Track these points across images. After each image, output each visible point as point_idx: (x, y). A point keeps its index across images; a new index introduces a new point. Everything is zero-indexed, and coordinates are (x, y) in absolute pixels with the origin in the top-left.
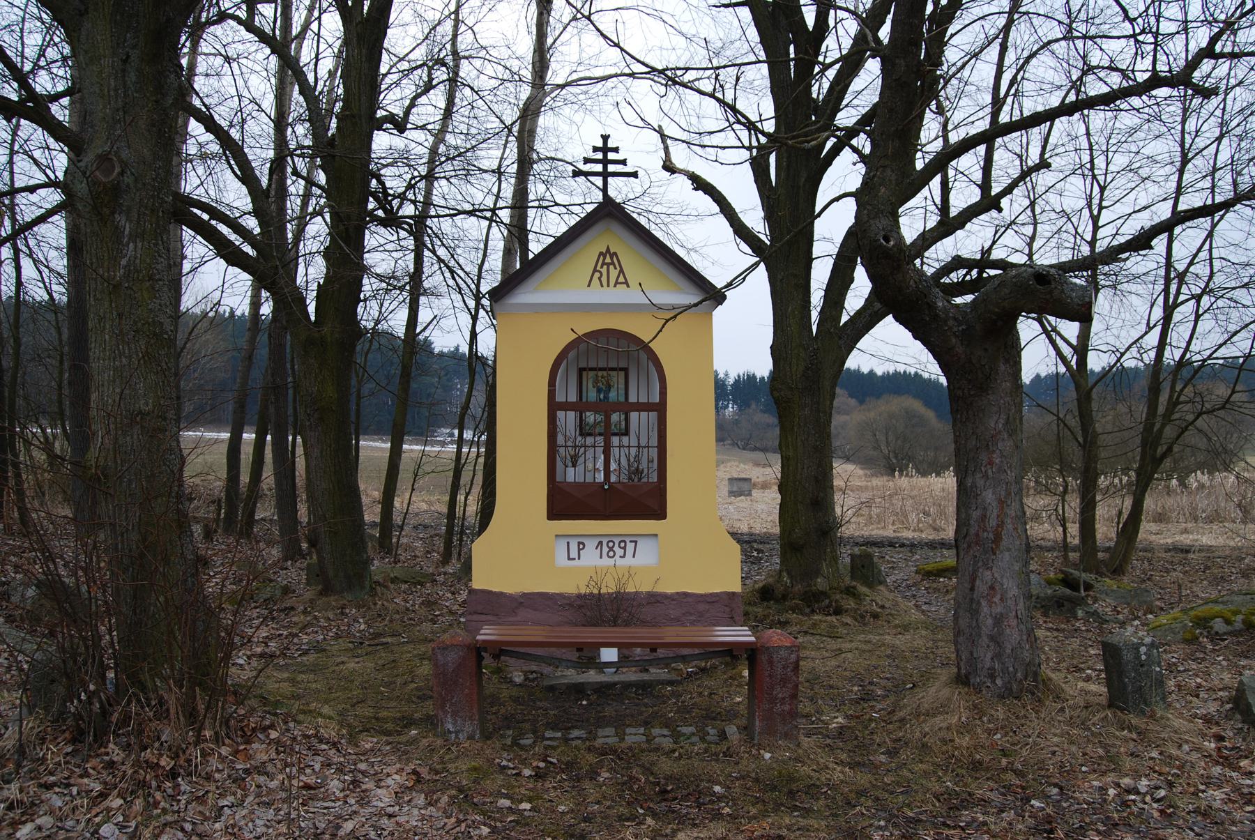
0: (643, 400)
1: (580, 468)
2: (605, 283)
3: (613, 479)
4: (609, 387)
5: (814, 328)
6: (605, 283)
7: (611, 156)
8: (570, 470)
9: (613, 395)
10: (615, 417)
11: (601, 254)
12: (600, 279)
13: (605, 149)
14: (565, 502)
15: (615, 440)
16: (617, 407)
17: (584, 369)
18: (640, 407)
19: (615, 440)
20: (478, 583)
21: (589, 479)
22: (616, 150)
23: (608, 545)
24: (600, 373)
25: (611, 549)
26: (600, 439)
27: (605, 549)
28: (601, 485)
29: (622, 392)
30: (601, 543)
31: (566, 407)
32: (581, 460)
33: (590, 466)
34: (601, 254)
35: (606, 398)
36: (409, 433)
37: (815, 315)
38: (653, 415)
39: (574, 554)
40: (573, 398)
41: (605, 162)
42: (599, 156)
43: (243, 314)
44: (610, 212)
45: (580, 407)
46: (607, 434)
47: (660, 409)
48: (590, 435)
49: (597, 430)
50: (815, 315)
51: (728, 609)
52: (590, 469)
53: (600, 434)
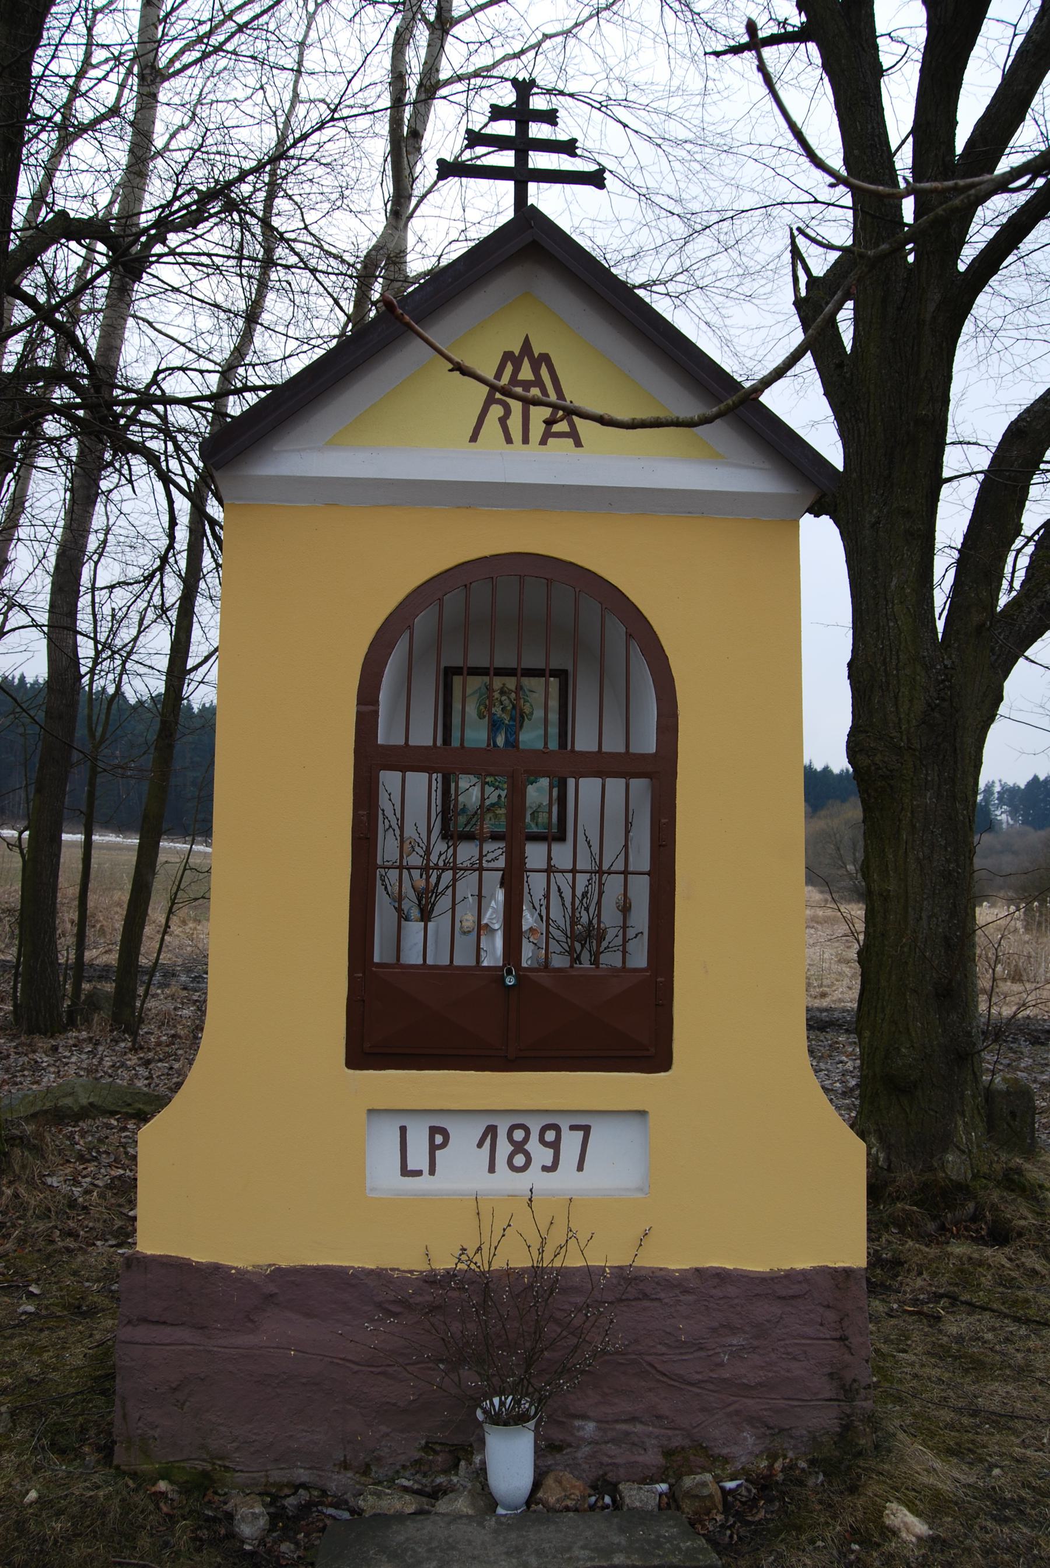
0: (613, 744)
1: (440, 924)
2: (516, 432)
3: (528, 954)
4: (519, 718)
5: (940, 625)
6: (516, 432)
7: (538, 131)
8: (414, 929)
9: (530, 737)
10: (538, 793)
11: (508, 356)
12: (503, 421)
13: (521, 113)
14: (398, 1020)
15: (535, 854)
16: (537, 765)
17: (457, 671)
18: (602, 765)
19: (535, 854)
20: (150, 1241)
21: (463, 959)
22: (550, 117)
23: (511, 1138)
24: (498, 682)
25: (519, 1147)
26: (496, 853)
27: (504, 1148)
28: (495, 975)
29: (554, 731)
30: (491, 1131)
31: (405, 759)
32: (444, 903)
33: (468, 919)
34: (508, 356)
35: (512, 743)
36: (165, 833)
37: (941, 597)
38: (640, 786)
39: (418, 1159)
40: (423, 736)
41: (522, 145)
42: (506, 128)
43: (36, 682)
44: (530, 245)
45: (443, 761)
46: (515, 837)
47: (659, 771)
48: (469, 837)
49: (489, 826)
50: (941, 597)
51: (831, 1316)
52: (465, 931)
53: (495, 837)
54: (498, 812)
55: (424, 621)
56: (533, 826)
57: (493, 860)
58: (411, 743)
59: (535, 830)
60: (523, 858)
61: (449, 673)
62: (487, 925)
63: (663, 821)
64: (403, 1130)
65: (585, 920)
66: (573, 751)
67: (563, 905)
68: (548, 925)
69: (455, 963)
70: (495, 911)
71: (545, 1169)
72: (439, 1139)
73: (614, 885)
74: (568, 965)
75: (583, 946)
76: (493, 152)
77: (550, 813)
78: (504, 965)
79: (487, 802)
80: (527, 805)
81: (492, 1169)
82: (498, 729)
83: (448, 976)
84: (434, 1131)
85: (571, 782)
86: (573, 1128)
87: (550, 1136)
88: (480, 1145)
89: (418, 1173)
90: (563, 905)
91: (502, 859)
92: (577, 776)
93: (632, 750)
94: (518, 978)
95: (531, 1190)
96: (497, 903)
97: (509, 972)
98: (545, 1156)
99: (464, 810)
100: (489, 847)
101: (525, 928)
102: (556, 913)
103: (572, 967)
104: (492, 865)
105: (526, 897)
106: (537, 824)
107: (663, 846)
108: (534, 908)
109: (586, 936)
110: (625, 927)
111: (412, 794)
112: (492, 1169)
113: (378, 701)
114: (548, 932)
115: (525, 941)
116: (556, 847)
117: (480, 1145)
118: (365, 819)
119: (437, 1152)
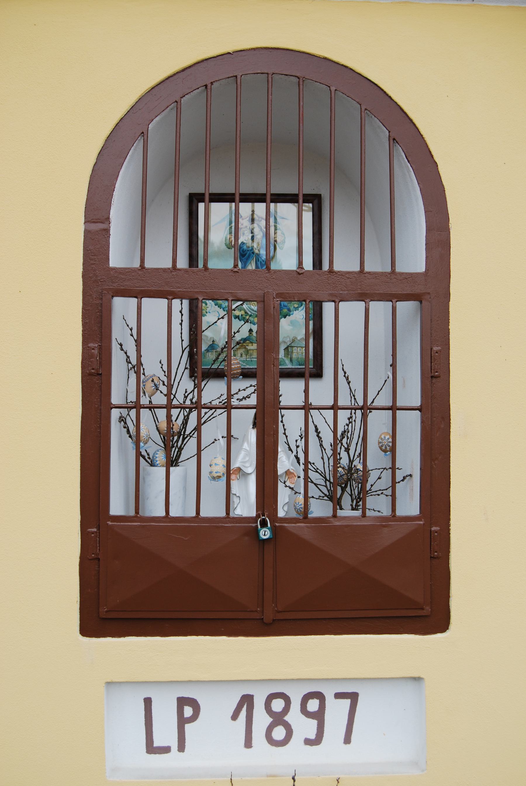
0: (376, 264)
3: (286, 503)
10: (293, 326)
15: (290, 391)
18: (364, 288)
19: (290, 391)
21: (212, 508)
25: (278, 719)
26: (245, 389)
28: (248, 528)
30: (247, 700)
31: (142, 284)
32: (190, 448)
38: (406, 309)
39: (165, 732)
46: (267, 374)
47: (428, 294)
49: (238, 361)
52: (208, 482)
53: (246, 374)
54: (250, 347)
55: (158, 128)
56: (287, 361)
57: (244, 398)
58: (147, 265)
59: (290, 366)
60: (277, 396)
61: (195, 199)
62: (239, 469)
63: (435, 349)
64: (148, 702)
65: (344, 461)
66: (331, 271)
67: (321, 445)
68: (306, 470)
69: (203, 514)
70: (248, 453)
71: (308, 742)
72: (188, 711)
73: (379, 423)
74: (330, 513)
75: (343, 490)
78: (258, 516)
79: (238, 337)
80: (281, 339)
81: (248, 743)
82: (247, 259)
83: (196, 528)
84: (182, 702)
85: (328, 308)
86: (339, 696)
87: (313, 705)
88: (235, 717)
89: (166, 750)
90: (321, 445)
91: (254, 397)
92: (337, 299)
93: (399, 269)
94: (274, 530)
95: (293, 779)
96: (250, 445)
97: (264, 524)
98: (310, 727)
99: (212, 346)
100: (237, 385)
101: (281, 470)
102: (314, 456)
103: (335, 516)
104: (244, 403)
105: (281, 438)
106: (291, 360)
107: (436, 377)
108: (290, 449)
109: (348, 482)
110: (393, 468)
111: (152, 329)
112: (248, 743)
113: (108, 218)
114: (307, 478)
115: (280, 486)
116: (313, 384)
117: (235, 717)
118: (96, 352)
119: (187, 727)
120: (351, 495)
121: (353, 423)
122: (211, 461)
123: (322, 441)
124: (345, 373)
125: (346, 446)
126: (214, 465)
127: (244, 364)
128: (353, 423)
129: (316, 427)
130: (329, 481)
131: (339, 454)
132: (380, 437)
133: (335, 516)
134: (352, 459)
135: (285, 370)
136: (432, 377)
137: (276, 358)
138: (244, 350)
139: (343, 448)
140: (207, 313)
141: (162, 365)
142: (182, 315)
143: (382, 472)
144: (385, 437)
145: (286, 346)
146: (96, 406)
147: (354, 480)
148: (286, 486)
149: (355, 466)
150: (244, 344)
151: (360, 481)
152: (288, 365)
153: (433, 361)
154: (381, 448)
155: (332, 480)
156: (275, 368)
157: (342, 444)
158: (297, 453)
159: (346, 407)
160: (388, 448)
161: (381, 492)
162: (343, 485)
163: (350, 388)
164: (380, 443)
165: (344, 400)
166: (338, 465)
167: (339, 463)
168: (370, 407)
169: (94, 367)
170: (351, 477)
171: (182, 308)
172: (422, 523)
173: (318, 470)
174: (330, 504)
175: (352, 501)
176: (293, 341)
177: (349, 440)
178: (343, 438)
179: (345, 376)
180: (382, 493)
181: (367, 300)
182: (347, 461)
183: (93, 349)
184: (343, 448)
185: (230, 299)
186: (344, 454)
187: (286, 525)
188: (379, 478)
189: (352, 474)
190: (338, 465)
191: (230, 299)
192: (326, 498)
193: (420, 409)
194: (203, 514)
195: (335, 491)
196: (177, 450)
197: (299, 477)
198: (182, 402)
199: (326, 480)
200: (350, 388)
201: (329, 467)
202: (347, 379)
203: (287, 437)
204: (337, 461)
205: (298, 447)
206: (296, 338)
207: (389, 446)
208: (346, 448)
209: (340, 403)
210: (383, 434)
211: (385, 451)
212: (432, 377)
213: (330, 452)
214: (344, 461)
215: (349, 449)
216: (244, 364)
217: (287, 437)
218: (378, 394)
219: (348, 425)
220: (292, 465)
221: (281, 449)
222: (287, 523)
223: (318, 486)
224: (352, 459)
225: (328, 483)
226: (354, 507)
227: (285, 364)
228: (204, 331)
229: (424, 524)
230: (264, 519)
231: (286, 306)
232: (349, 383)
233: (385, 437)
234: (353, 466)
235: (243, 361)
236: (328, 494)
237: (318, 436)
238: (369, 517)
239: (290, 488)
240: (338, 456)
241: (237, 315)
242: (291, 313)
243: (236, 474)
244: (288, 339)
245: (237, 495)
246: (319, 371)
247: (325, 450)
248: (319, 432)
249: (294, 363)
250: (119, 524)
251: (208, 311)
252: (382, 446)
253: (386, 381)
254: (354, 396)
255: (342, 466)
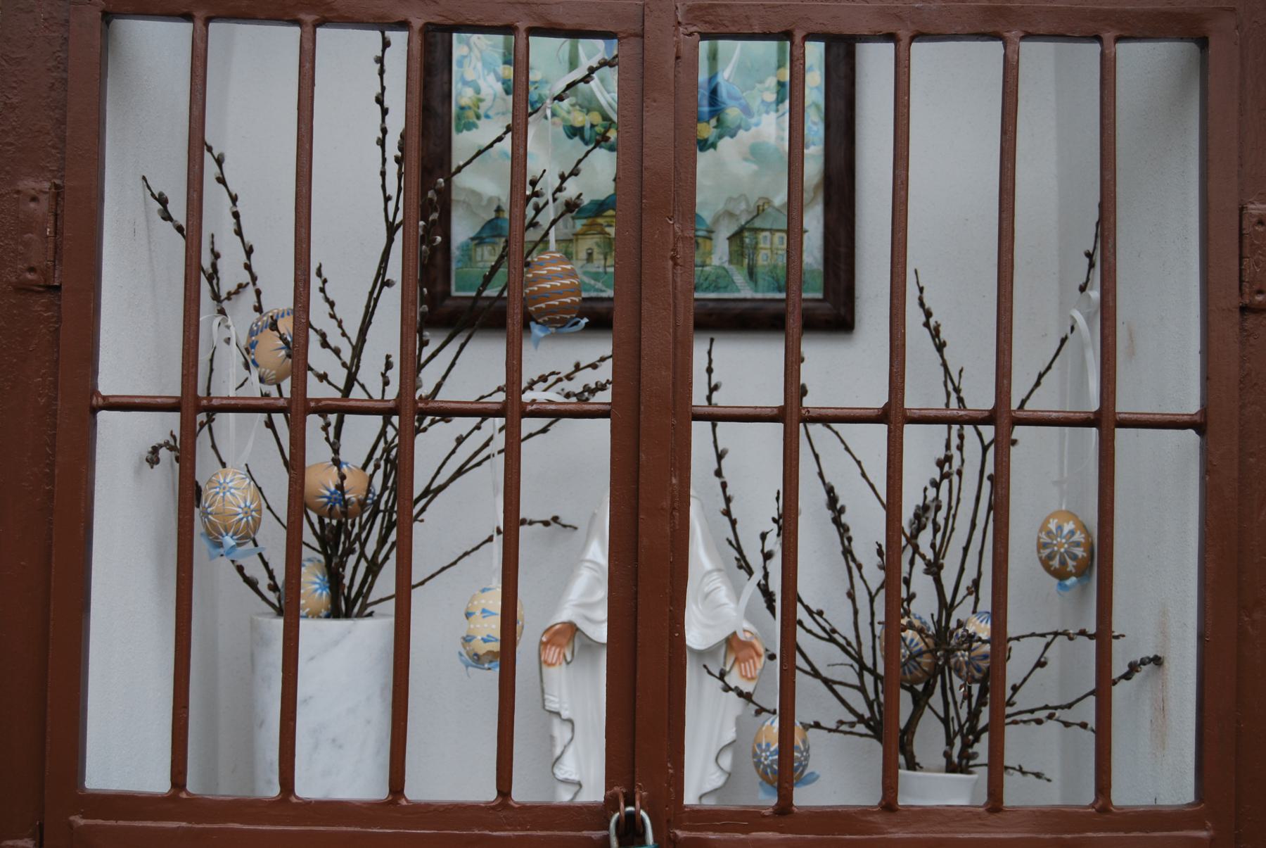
15: (741, 370)
21: (452, 772)
56: (739, 277)
59: (747, 293)
67: (847, 553)
68: (789, 625)
69: (415, 791)
73: (1049, 476)
74: (870, 796)
75: (920, 702)
76: (866, 735)
77: (794, 232)
78: (611, 803)
85: (875, 62)
90: (847, 553)
92: (903, 34)
102: (819, 580)
103: (889, 804)
106: (752, 273)
109: (931, 679)
110: (1104, 637)
114: (790, 646)
118: (42, 208)
120: (946, 721)
121: (955, 478)
122: (471, 601)
123: (850, 539)
124: (928, 314)
125: (930, 555)
126: (478, 613)
127: (599, 285)
128: (955, 478)
129: (830, 490)
130: (873, 672)
131: (907, 582)
132: (1044, 527)
133: (889, 804)
134: (949, 599)
135: (732, 305)
136: (1244, 309)
137: (684, 238)
138: (597, 238)
139: (919, 561)
140: (478, 117)
141: (325, 281)
142: (385, 112)
143: (1048, 645)
144: (1060, 528)
145: (734, 228)
146: (43, 401)
147: (958, 671)
148: (727, 688)
149: (960, 624)
150: (600, 220)
151: (977, 675)
152: (743, 290)
153: (1247, 251)
154: (1046, 563)
155: (881, 670)
156: (679, 270)
157: (916, 549)
158: (766, 576)
159: (932, 413)
160: (1071, 564)
161: (1047, 712)
162: (920, 687)
163: (944, 365)
164: (1045, 545)
165: (923, 392)
166: (904, 621)
167: (907, 613)
168: (1021, 414)
169: (34, 264)
170: (947, 661)
171: (383, 88)
172: (1203, 834)
173: (836, 636)
174: (877, 748)
175: (950, 742)
176: (759, 211)
177: (939, 535)
178: (921, 527)
179: (927, 325)
180: (1050, 717)
181: (1014, 34)
182: (934, 607)
183: (34, 199)
184: (920, 565)
185: (522, 25)
186: (922, 583)
187: (711, 836)
188: (1041, 664)
189: (950, 653)
190: (904, 621)
191: (522, 25)
192: (861, 728)
193: (1198, 425)
194: (415, 791)
195: (892, 706)
196: (363, 565)
197: (772, 657)
198: (377, 396)
199: (863, 667)
200: (944, 365)
201: (872, 624)
202: (935, 333)
203: (733, 523)
204: (897, 604)
205: (767, 556)
206: (768, 202)
207: (1074, 557)
208: (928, 563)
209: (912, 402)
210: (1052, 516)
211: (1061, 574)
212: (1244, 309)
213: (875, 577)
214: (924, 606)
215: (941, 567)
216: (599, 285)
217: (733, 523)
218: (1038, 384)
219: (936, 485)
220: (749, 615)
221: (704, 557)
222: (715, 829)
223: (836, 687)
224: (949, 599)
225: (869, 679)
226: (956, 759)
227: (730, 285)
228: (459, 169)
229: (1212, 840)
230: (631, 817)
231: (737, 99)
232: (940, 347)
233: (1060, 528)
234: (953, 624)
235: (596, 276)
236: (867, 714)
237: (837, 521)
238: (1014, 810)
239: (740, 694)
240: (904, 588)
241: (578, 125)
242: (753, 121)
243: (560, 646)
244: (743, 206)
245: (565, 714)
246: (842, 311)
247: (859, 567)
248: (842, 510)
249: (760, 282)
250: (112, 823)
251: (482, 112)
252: (1051, 557)
253: (1063, 341)
254: (957, 390)
255: (917, 623)
